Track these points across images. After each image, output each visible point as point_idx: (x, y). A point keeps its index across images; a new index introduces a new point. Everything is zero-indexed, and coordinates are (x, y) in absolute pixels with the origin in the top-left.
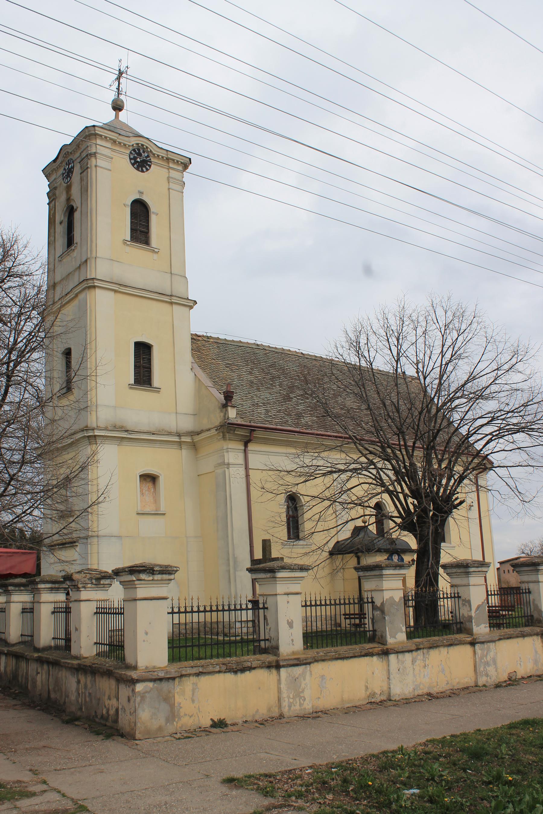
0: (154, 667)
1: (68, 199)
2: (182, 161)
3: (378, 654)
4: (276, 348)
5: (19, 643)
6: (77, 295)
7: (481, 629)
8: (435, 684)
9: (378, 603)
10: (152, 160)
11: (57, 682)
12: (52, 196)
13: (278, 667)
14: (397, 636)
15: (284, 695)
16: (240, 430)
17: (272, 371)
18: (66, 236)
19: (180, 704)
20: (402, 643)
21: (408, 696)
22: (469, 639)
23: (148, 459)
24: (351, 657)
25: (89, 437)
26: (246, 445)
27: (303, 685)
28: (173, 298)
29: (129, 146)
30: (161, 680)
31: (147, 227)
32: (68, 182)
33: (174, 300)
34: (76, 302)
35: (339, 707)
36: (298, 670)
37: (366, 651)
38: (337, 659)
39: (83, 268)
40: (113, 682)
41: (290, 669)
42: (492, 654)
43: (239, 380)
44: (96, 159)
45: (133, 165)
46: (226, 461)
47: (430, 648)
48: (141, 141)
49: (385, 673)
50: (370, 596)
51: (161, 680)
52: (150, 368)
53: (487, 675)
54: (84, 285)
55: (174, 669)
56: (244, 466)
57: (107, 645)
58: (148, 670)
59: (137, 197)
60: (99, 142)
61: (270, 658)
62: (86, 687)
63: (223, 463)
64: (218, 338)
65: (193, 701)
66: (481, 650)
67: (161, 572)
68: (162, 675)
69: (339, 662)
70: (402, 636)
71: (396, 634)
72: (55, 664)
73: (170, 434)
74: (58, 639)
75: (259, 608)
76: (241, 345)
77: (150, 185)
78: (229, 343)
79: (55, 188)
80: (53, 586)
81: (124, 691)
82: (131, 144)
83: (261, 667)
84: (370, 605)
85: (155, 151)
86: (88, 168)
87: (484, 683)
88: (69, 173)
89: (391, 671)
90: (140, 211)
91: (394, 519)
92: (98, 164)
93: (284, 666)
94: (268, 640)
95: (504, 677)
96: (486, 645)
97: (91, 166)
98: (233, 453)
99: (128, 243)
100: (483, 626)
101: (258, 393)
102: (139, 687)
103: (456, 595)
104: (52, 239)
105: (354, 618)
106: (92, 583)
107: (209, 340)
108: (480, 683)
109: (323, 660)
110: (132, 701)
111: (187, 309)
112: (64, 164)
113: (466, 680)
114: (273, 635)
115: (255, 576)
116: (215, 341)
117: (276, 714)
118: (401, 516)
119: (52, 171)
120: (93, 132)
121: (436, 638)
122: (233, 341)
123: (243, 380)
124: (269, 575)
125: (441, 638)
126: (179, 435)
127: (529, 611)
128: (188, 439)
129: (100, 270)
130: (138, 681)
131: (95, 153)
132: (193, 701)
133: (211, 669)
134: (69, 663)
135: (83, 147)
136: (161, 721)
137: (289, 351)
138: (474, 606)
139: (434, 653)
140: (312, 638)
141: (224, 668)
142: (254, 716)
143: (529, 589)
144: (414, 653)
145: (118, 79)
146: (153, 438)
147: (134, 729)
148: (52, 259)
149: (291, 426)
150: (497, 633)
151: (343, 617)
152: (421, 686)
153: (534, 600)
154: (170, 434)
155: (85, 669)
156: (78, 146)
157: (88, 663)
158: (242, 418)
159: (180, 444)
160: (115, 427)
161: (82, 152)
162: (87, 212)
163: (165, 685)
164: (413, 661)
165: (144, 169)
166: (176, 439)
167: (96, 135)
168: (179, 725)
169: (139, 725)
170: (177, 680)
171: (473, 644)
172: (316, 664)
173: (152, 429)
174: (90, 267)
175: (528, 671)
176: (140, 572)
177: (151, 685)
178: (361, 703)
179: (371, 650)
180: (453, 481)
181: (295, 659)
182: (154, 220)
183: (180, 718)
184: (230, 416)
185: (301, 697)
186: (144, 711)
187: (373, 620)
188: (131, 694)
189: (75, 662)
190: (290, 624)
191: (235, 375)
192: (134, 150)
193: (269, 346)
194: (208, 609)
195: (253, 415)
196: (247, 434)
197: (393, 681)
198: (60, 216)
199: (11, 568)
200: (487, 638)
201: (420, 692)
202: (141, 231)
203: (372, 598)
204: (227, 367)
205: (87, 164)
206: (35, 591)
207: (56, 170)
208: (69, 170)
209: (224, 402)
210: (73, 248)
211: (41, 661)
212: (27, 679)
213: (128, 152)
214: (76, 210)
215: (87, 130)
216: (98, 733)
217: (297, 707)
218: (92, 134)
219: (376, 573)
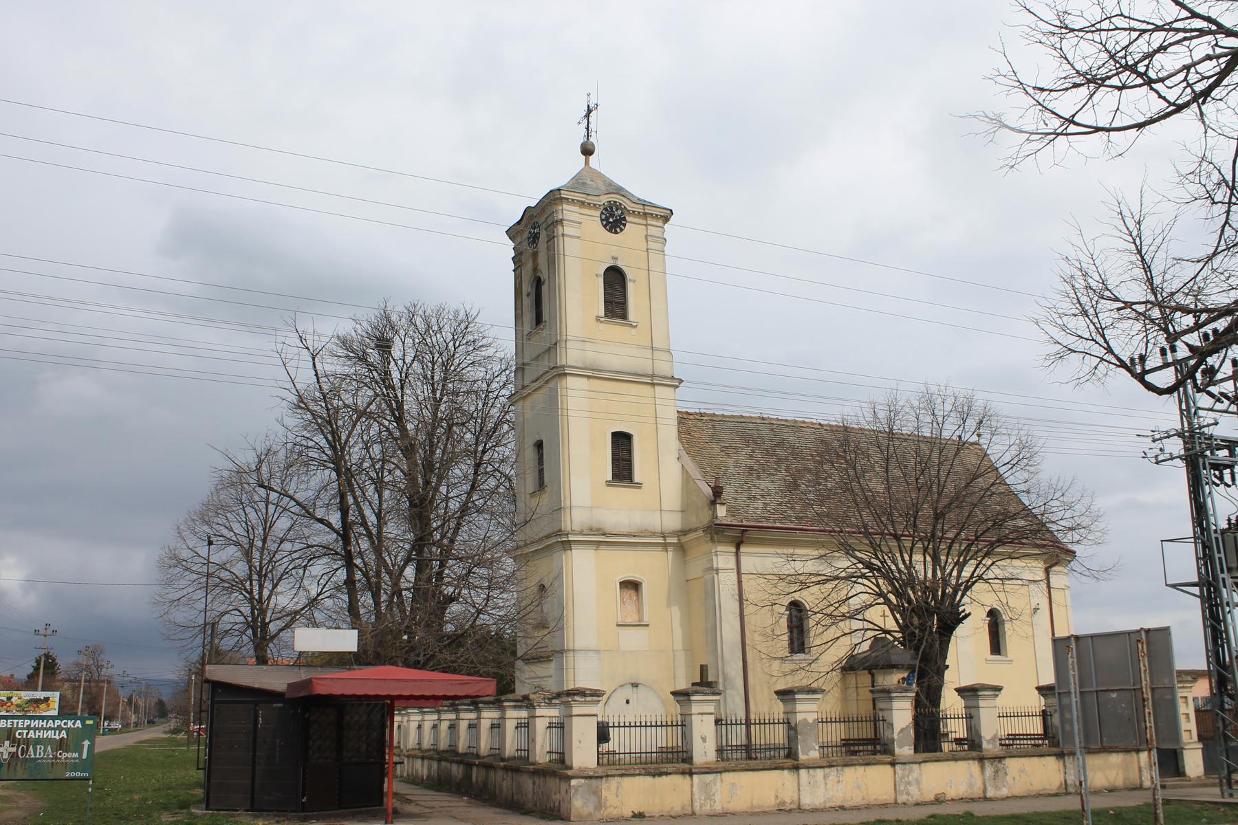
1: (535, 269)
3: (789, 768)
12: (516, 260)
13: (691, 774)
15: (696, 797)
17: (779, 452)
23: (628, 564)
26: (738, 548)
30: (591, 777)
31: (624, 297)
34: (545, 390)
42: (915, 775)
43: (735, 466)
45: (605, 226)
51: (591, 777)
53: (908, 794)
54: (555, 372)
55: (601, 771)
58: (580, 770)
61: (686, 766)
63: (711, 568)
64: (714, 415)
67: (591, 695)
68: (591, 774)
69: (750, 773)
70: (814, 754)
72: (517, 770)
77: (625, 247)
79: (521, 254)
81: (564, 786)
85: (630, 206)
88: (535, 238)
90: (615, 279)
98: (724, 558)
101: (757, 482)
102: (574, 782)
108: (899, 801)
117: (689, 811)
122: (733, 416)
126: (664, 537)
128: (675, 541)
129: (572, 355)
133: (632, 772)
136: (591, 809)
146: (634, 540)
148: (520, 336)
154: (653, 534)
159: (665, 546)
163: (594, 782)
164: (825, 777)
171: (893, 764)
173: (633, 530)
182: (630, 287)
190: (704, 739)
191: (731, 461)
192: (606, 209)
196: (739, 536)
197: (803, 793)
198: (527, 287)
208: (535, 233)
211: (506, 769)
217: (708, 807)
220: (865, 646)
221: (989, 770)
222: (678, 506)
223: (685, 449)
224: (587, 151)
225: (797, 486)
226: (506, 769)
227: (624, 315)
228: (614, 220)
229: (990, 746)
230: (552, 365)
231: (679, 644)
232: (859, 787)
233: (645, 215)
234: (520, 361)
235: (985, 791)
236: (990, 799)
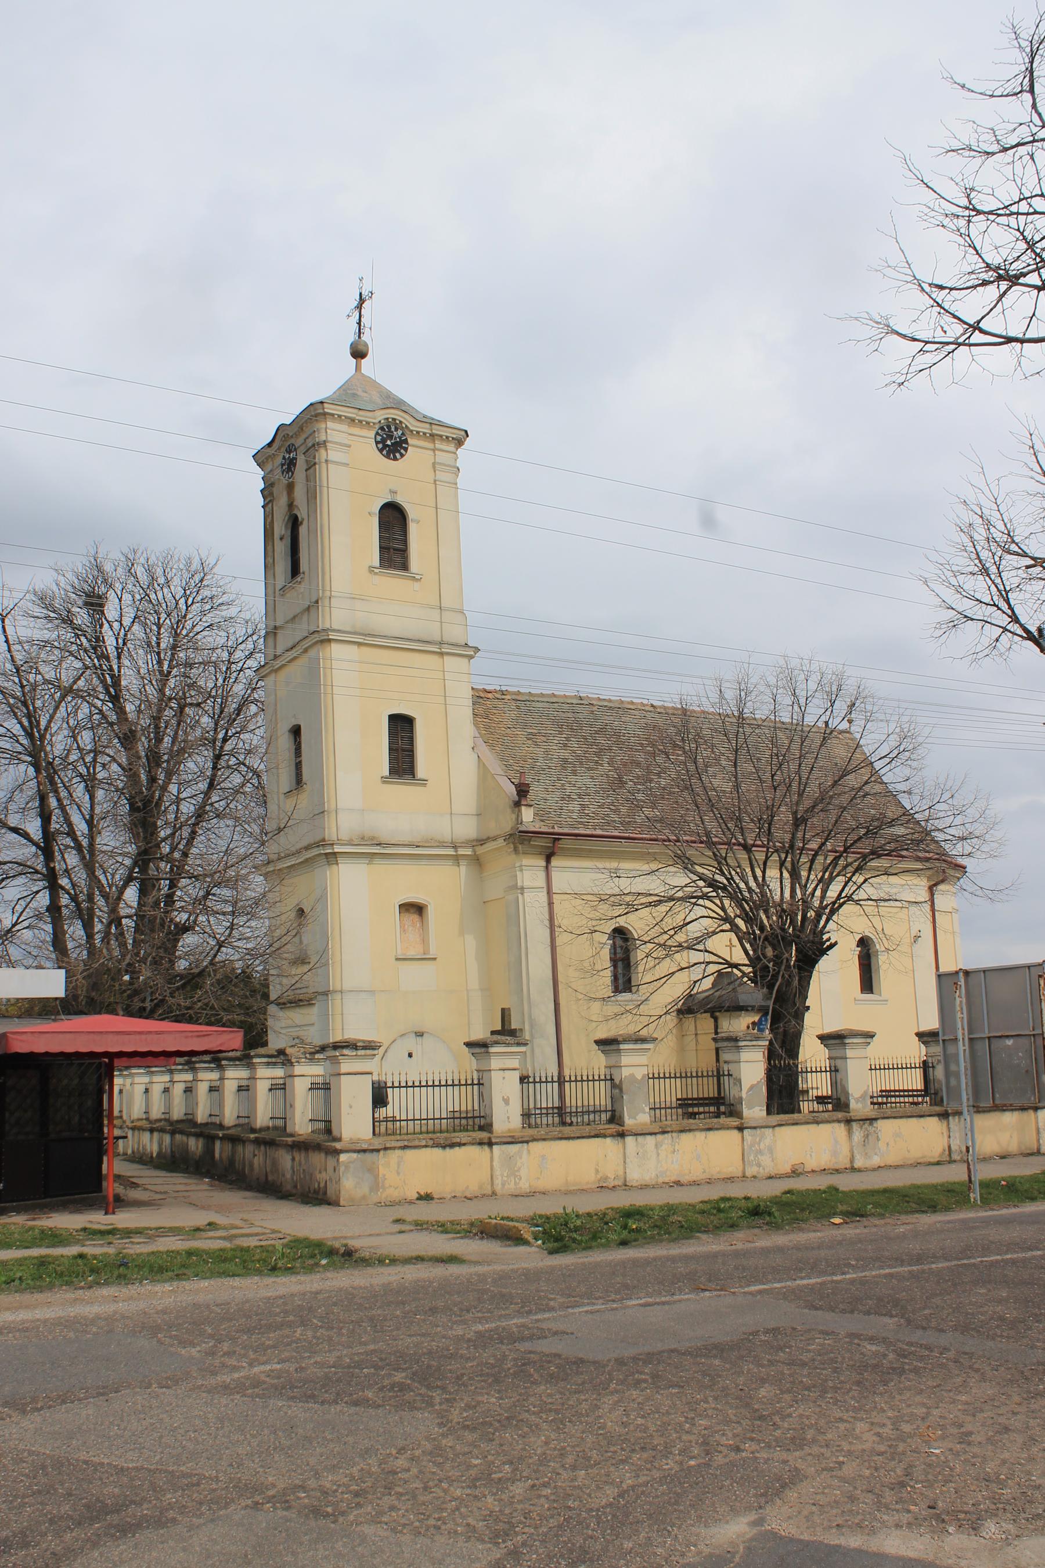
1: (291, 505)
3: (612, 1136)
4: (610, 701)
5: (235, 1126)
6: (306, 651)
9: (617, 1081)
10: (409, 440)
11: (275, 1163)
12: (268, 493)
15: (498, 1172)
18: (289, 558)
20: (645, 1124)
24: (578, 1138)
25: (326, 854)
26: (548, 860)
27: (519, 1164)
30: (364, 1151)
36: (513, 1149)
37: (596, 1132)
38: (561, 1139)
40: (323, 1155)
42: (767, 1141)
45: (381, 451)
46: (519, 884)
48: (392, 414)
49: (621, 1156)
51: (364, 1151)
52: (412, 751)
53: (759, 1165)
54: (316, 637)
55: (377, 1143)
56: (545, 890)
59: (388, 499)
60: (330, 424)
61: (484, 1135)
63: (515, 887)
64: (519, 693)
65: (398, 1173)
67: (365, 1048)
68: (365, 1146)
69: (564, 1142)
77: (406, 479)
78: (536, 699)
79: (272, 485)
80: (270, 1060)
81: (331, 1162)
82: (376, 421)
85: (413, 425)
86: (315, 464)
87: (755, 1174)
88: (290, 465)
90: (393, 518)
92: (330, 458)
93: (496, 1144)
95: (787, 1169)
96: (758, 1131)
98: (530, 872)
100: (757, 1109)
101: (572, 779)
102: (343, 1157)
104: (270, 560)
108: (747, 1174)
109: (544, 1140)
111: (466, 660)
112: (283, 449)
113: (730, 1169)
116: (514, 697)
119: (267, 459)
120: (321, 411)
124: (483, 1050)
126: (455, 847)
128: (468, 852)
129: (337, 616)
130: (342, 1151)
132: (398, 1173)
133: (416, 1143)
135: (308, 431)
136: (365, 1189)
137: (632, 703)
138: (746, 1085)
141: (431, 1143)
144: (659, 1136)
145: (360, 307)
146: (416, 851)
147: (338, 1197)
150: (775, 1119)
152: (668, 1173)
154: (442, 845)
155: (303, 1146)
156: (301, 428)
157: (301, 1139)
159: (456, 859)
160: (363, 838)
163: (368, 1156)
165: (398, 455)
166: (451, 852)
167: (325, 414)
168: (384, 1196)
169: (343, 1193)
170: (382, 1152)
171: (741, 1129)
172: (535, 1143)
176: (343, 1047)
177: (355, 1155)
178: (589, 1186)
182: (414, 531)
189: (290, 1139)
190: (506, 1101)
192: (382, 428)
193: (599, 699)
196: (550, 846)
199: (221, 1045)
200: (760, 1123)
202: (394, 549)
205: (314, 458)
206: (251, 1066)
208: (290, 457)
209: (517, 798)
210: (299, 579)
211: (258, 1142)
212: (244, 1164)
213: (372, 434)
214: (301, 523)
215: (312, 408)
216: (307, 1203)
217: (512, 1185)
224: (358, 353)
225: (622, 783)
226: (258, 1142)
227: (405, 566)
228: (392, 443)
229: (860, 1105)
230: (313, 628)
231: (474, 982)
234: (272, 624)
235: (852, 1161)
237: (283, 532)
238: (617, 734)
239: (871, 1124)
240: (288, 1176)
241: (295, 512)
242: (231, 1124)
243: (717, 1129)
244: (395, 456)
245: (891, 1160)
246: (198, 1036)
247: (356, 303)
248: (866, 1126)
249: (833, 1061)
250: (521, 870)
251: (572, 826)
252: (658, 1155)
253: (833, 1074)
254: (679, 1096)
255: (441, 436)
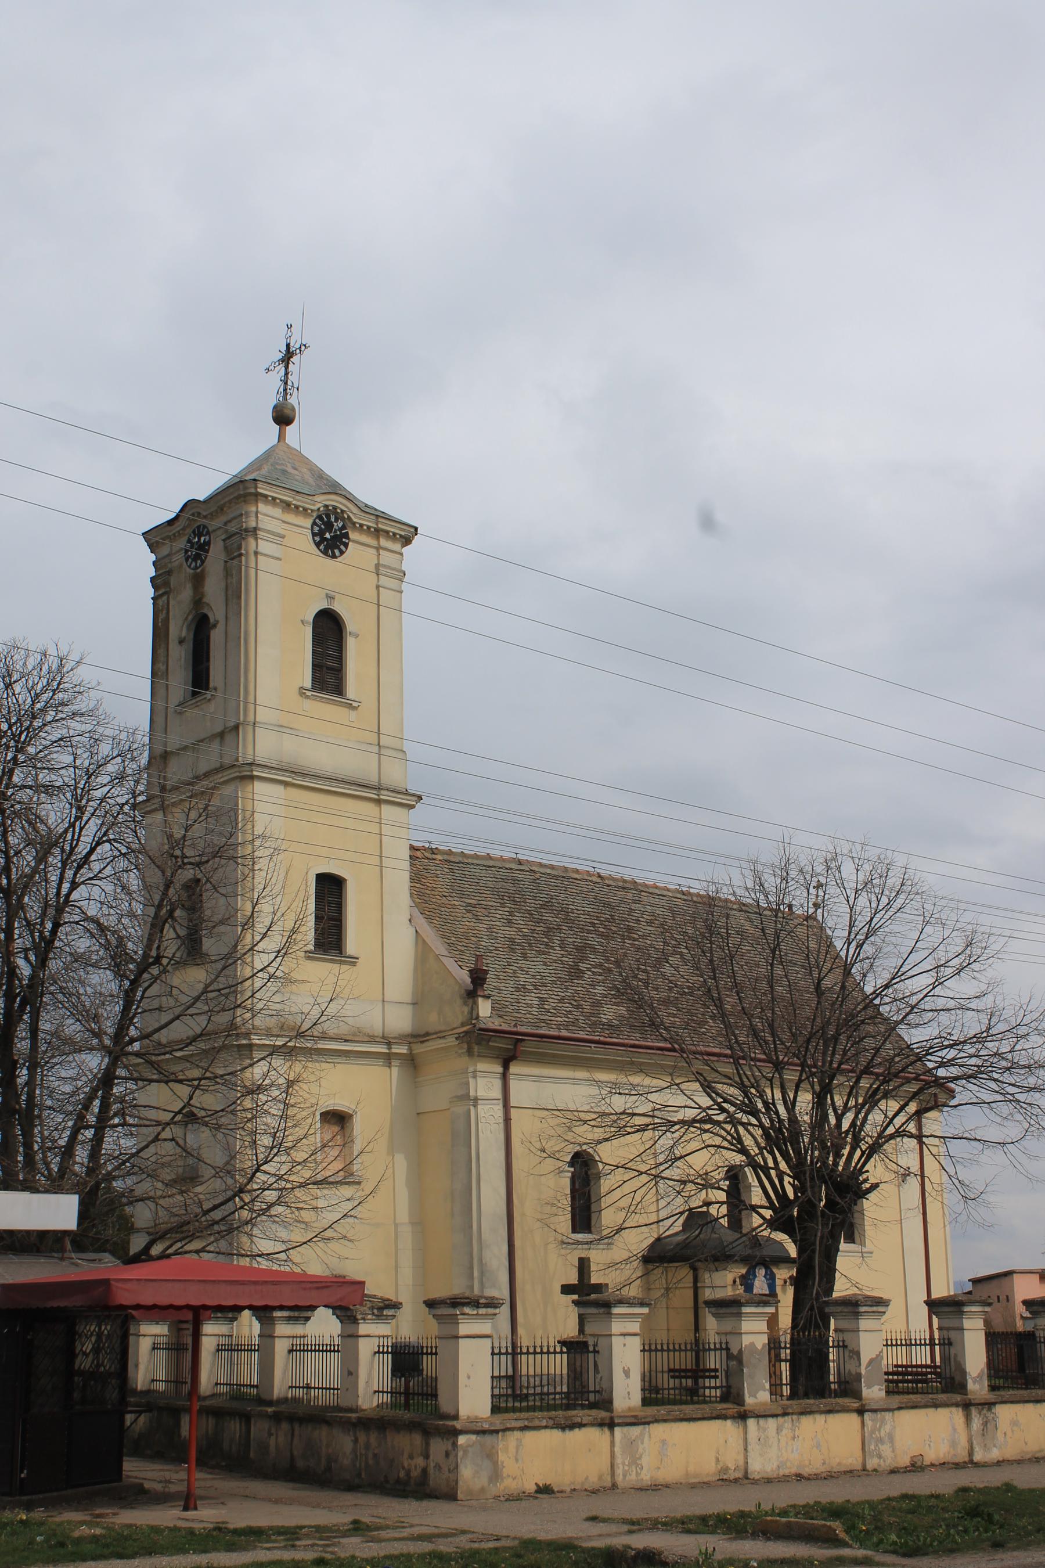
0: (476, 1418)
1: (198, 601)
2: (403, 533)
3: (733, 1418)
4: (552, 867)
7: (873, 1392)
8: (807, 1463)
10: (352, 535)
12: (161, 583)
14: (758, 1395)
15: (619, 1460)
16: (498, 1039)
19: (503, 1462)
20: (765, 1404)
21: (770, 1475)
22: (856, 1405)
26: (506, 1066)
27: (640, 1450)
28: (382, 792)
29: (312, 511)
32: (196, 568)
33: (385, 796)
35: (683, 1481)
39: (229, 738)
41: (626, 1429)
42: (887, 1428)
44: (256, 539)
45: (318, 545)
46: (472, 1093)
47: (802, 1413)
48: (333, 501)
49: (741, 1442)
50: (724, 1341)
52: (340, 921)
53: (880, 1457)
56: (501, 1102)
57: (387, 1392)
59: (324, 605)
60: (262, 507)
61: (603, 1414)
62: (367, 1446)
63: (466, 1097)
66: (872, 1420)
67: (487, 1306)
68: (486, 1426)
71: (757, 1393)
73: (372, 1039)
74: (296, 1387)
75: (588, 1352)
76: (491, 863)
78: (470, 861)
79: (169, 573)
80: (292, 1314)
81: (438, 1447)
82: (315, 508)
83: (592, 1425)
84: (724, 1352)
86: (241, 555)
87: (876, 1467)
88: (198, 552)
89: (749, 1440)
90: (329, 629)
91: (760, 1210)
92: (260, 549)
93: (619, 1425)
94: (598, 1392)
95: (905, 1461)
96: (879, 1415)
97: (247, 552)
98: (485, 1083)
99: (309, 693)
100: (876, 1388)
101: (523, 964)
102: (462, 1440)
103: (841, 1344)
105: (686, 1377)
106: (373, 1314)
107: (434, 856)
108: (869, 1467)
109: (665, 1421)
110: (451, 1457)
112: (189, 531)
113: (850, 1461)
114: (605, 1386)
115: (583, 1311)
116: (446, 857)
117: (607, 1482)
118: (771, 1206)
120: (253, 490)
121: (811, 1401)
122: (476, 856)
123: (496, 938)
124: (602, 1310)
125: (817, 1402)
126: (389, 1044)
127: (948, 1371)
128: (403, 1050)
129: (264, 745)
131: (255, 529)
132: (517, 1460)
133: (536, 1423)
134: (341, 1417)
136: (483, 1481)
137: (577, 871)
139: (806, 1421)
140: (652, 1395)
141: (551, 1423)
142: (583, 1484)
143: (949, 1339)
144: (780, 1419)
149: (583, 1029)
150: (896, 1400)
151: (666, 1375)
152: (788, 1464)
153: (955, 1355)
154: (372, 1039)
158: (500, 1016)
159: (388, 1058)
161: (230, 521)
162: (240, 638)
163: (488, 1439)
164: (779, 1430)
165: (337, 552)
166: (383, 1049)
167: (257, 495)
168: (502, 1488)
169: (460, 1483)
171: (861, 1412)
172: (656, 1425)
174: (244, 740)
175: (942, 1455)
176: (464, 1304)
177: (473, 1437)
179: (724, 1412)
180: (858, 1153)
181: (633, 1416)
182: (351, 645)
183: (502, 1479)
184: (481, 1014)
185: (638, 1465)
186: (466, 1467)
187: (727, 1372)
188: (450, 1448)
190: (627, 1373)
191: (482, 927)
192: (320, 517)
193: (540, 865)
194: (531, 1350)
195: (517, 1011)
196: (509, 1049)
197: (752, 1455)
198: (177, 628)
201: (786, 1472)
203: (727, 1343)
204: (469, 911)
205: (240, 547)
207: (173, 538)
209: (471, 987)
211: (277, 1418)
214: (215, 626)
215: (241, 486)
217: (633, 1477)
218: (251, 494)
219: (734, 1310)
220: (678, 1227)
221: (977, 1422)
222: (408, 997)
223: (417, 905)
224: (283, 418)
225: (578, 974)
226: (277, 1418)
227: (339, 689)
228: (331, 534)
229: (977, 1387)
230: (227, 761)
231: (403, 1215)
232: (818, 1446)
233: (377, 533)
234: (159, 749)
235: (971, 1453)
236: (977, 1465)
237: (184, 634)
238: (565, 911)
239: (990, 1409)
240: (346, 1462)
241: (205, 611)
242: (208, 1393)
243: (838, 1412)
244: (333, 553)
245: (1010, 1453)
246: (318, 1288)
247: (280, 356)
248: (985, 1411)
249: (945, 1332)
250: (475, 1077)
251: (533, 1025)
252: (779, 1440)
253: (947, 1347)
254: (672, 1367)
255: (387, 532)
